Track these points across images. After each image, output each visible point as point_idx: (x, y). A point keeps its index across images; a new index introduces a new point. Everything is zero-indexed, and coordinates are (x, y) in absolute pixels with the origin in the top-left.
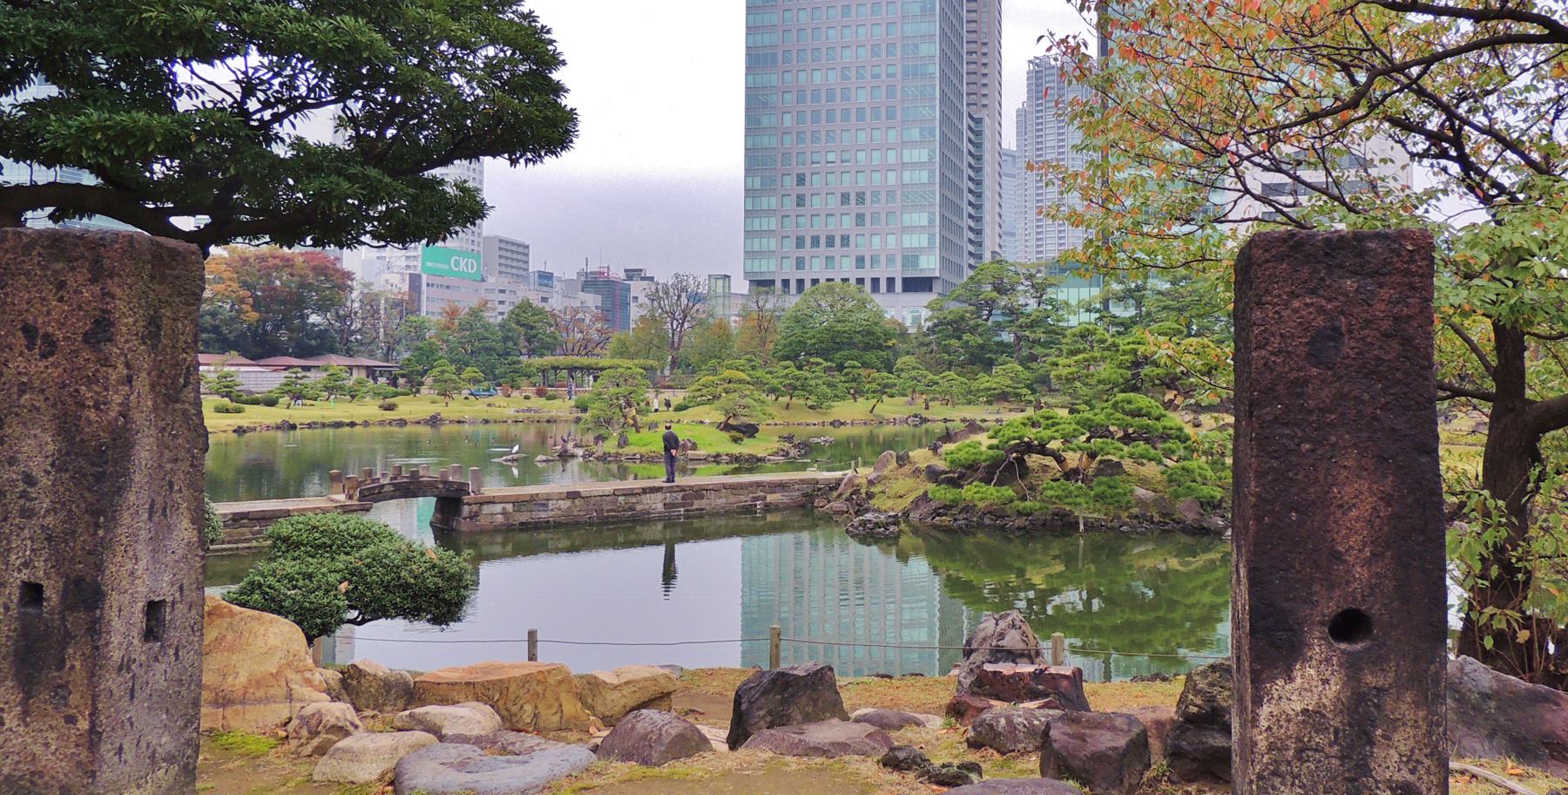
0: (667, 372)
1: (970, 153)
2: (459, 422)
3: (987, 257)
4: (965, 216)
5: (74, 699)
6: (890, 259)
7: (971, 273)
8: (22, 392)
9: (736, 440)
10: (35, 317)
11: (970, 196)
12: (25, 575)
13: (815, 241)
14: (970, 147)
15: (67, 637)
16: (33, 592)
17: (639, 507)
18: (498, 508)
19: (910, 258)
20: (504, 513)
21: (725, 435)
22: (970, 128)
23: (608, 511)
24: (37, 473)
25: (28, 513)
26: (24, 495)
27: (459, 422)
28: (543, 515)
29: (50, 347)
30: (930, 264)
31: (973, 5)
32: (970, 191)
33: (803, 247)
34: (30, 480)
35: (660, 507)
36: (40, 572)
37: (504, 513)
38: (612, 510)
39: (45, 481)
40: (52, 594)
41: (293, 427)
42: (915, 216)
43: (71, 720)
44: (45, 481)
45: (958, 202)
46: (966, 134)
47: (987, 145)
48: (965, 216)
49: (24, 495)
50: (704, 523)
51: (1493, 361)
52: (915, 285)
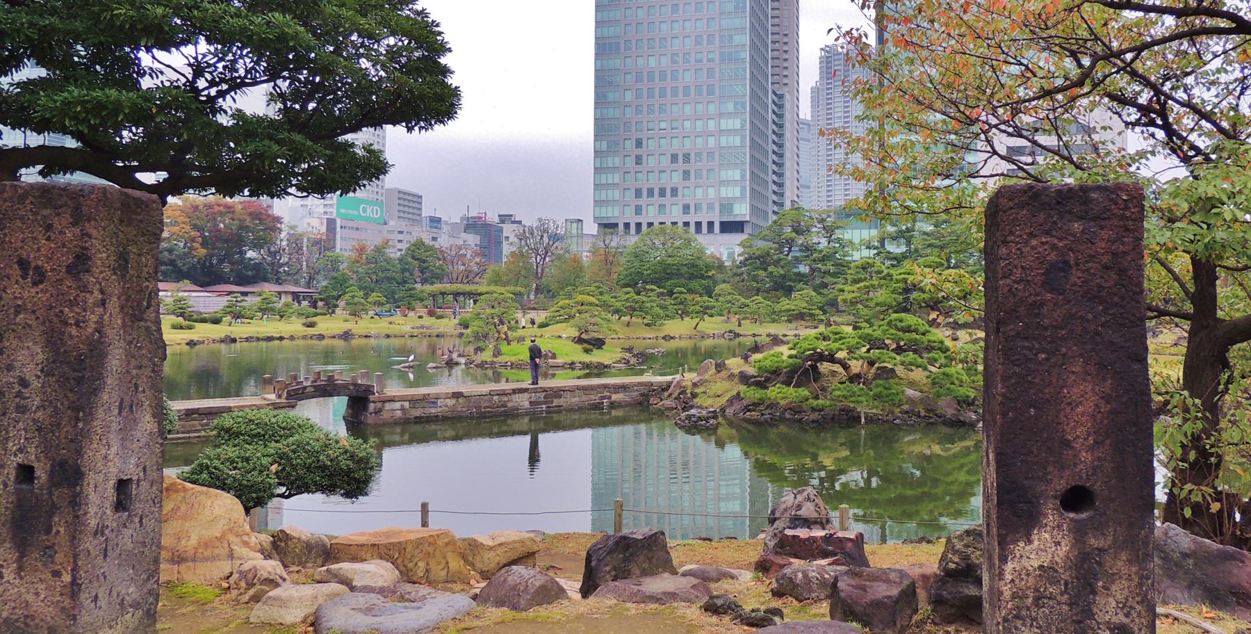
0: (532, 297)
1: (774, 122)
2: (366, 337)
3: (788, 205)
4: (770, 172)
5: (59, 558)
6: (710, 207)
7: (775, 218)
9: (587, 351)
10: (28, 253)
11: (774, 157)
12: (20, 459)
13: (651, 192)
14: (774, 117)
15: (54, 508)
16: (26, 472)
17: (510, 405)
18: (397, 405)
19: (726, 206)
20: (402, 409)
21: (579, 347)
22: (774, 102)
23: (485, 407)
24: (30, 377)
25: (22, 409)
26: (19, 394)
27: (366, 337)
28: (433, 411)
29: (40, 277)
30: (742, 211)
31: (776, 4)
32: (774, 152)
33: (641, 197)
34: (24, 383)
35: (527, 404)
37: (402, 409)
38: (489, 407)
39: (36, 384)
40: (41, 474)
41: (234, 341)
42: (730, 173)
43: (57, 574)
44: (36, 384)
45: (764, 161)
46: (771, 107)
47: (788, 116)
48: (770, 172)
49: (19, 394)
50: (562, 417)
51: (1191, 288)
52: (730, 227)
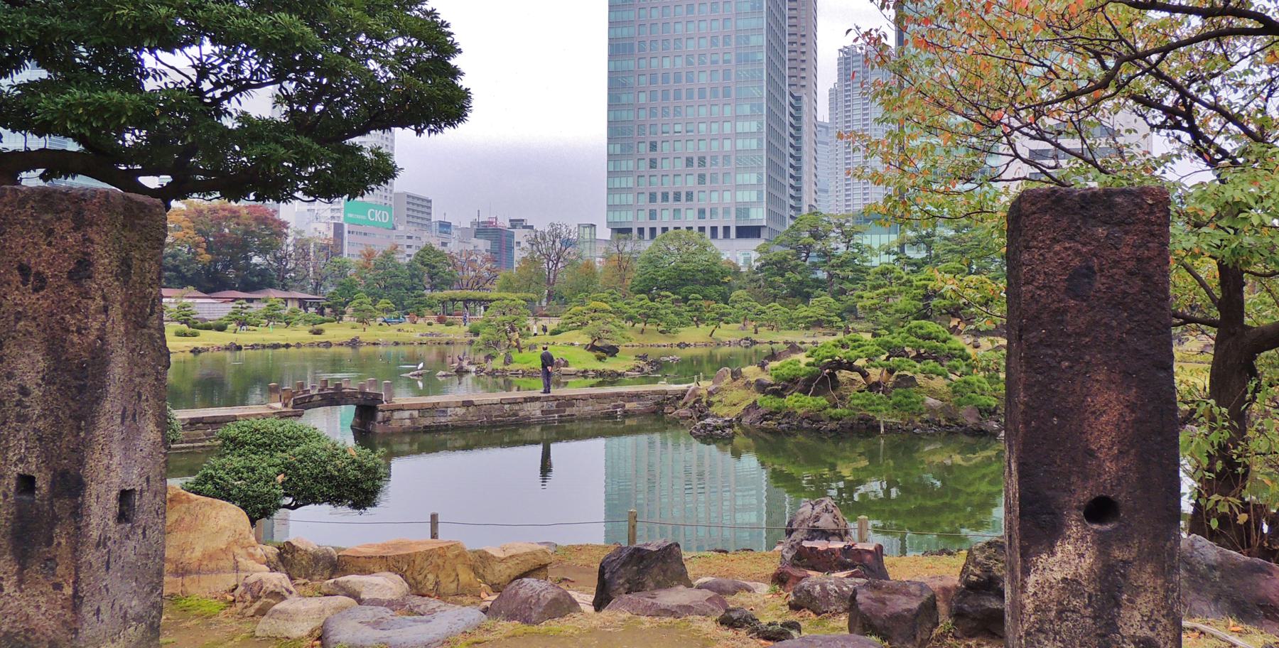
1: (791, 125)
2: (374, 344)
3: (805, 210)
4: (787, 176)
6: (726, 211)
7: (792, 222)
8: (18, 320)
9: (600, 359)
10: (29, 258)
11: (791, 160)
12: (20, 469)
14: (791, 119)
15: (55, 519)
16: (27, 483)
17: (521, 414)
18: (406, 414)
19: (743, 210)
20: (411, 418)
21: (592, 355)
22: (791, 104)
23: (496, 416)
24: (30, 385)
25: (22, 418)
26: (19, 403)
27: (374, 344)
28: (443, 420)
29: (41, 283)
30: (758, 216)
31: (794, 4)
32: (791, 156)
33: (655, 201)
34: (24, 391)
35: (538, 413)
36: (33, 466)
37: (411, 418)
38: (500, 416)
39: (37, 392)
40: (42, 484)
41: (239, 348)
43: (58, 587)
44: (37, 392)
45: (781, 164)
47: (805, 118)
48: (787, 176)
49: (19, 403)
52: (746, 232)
